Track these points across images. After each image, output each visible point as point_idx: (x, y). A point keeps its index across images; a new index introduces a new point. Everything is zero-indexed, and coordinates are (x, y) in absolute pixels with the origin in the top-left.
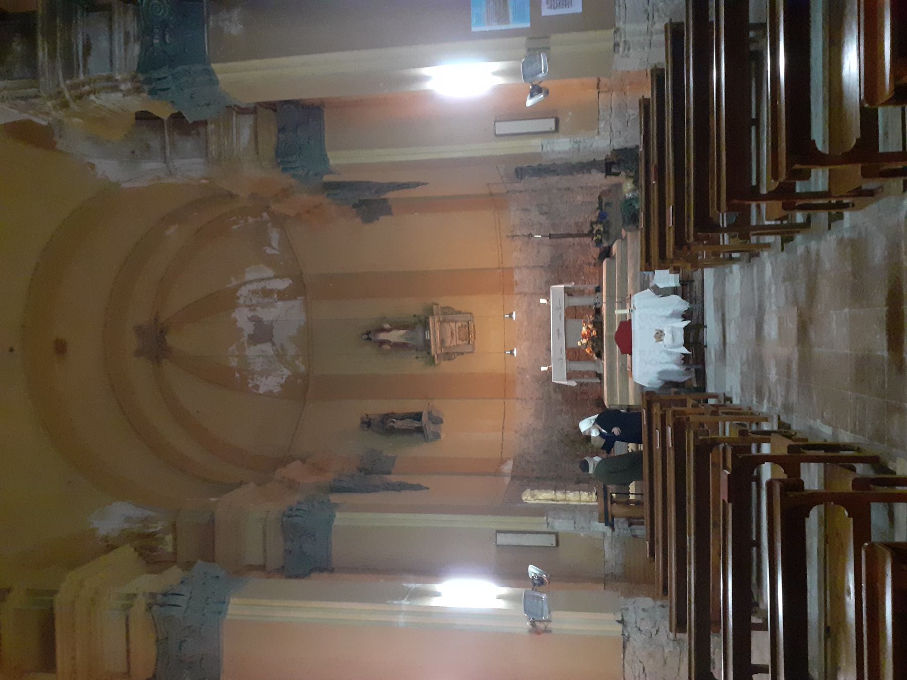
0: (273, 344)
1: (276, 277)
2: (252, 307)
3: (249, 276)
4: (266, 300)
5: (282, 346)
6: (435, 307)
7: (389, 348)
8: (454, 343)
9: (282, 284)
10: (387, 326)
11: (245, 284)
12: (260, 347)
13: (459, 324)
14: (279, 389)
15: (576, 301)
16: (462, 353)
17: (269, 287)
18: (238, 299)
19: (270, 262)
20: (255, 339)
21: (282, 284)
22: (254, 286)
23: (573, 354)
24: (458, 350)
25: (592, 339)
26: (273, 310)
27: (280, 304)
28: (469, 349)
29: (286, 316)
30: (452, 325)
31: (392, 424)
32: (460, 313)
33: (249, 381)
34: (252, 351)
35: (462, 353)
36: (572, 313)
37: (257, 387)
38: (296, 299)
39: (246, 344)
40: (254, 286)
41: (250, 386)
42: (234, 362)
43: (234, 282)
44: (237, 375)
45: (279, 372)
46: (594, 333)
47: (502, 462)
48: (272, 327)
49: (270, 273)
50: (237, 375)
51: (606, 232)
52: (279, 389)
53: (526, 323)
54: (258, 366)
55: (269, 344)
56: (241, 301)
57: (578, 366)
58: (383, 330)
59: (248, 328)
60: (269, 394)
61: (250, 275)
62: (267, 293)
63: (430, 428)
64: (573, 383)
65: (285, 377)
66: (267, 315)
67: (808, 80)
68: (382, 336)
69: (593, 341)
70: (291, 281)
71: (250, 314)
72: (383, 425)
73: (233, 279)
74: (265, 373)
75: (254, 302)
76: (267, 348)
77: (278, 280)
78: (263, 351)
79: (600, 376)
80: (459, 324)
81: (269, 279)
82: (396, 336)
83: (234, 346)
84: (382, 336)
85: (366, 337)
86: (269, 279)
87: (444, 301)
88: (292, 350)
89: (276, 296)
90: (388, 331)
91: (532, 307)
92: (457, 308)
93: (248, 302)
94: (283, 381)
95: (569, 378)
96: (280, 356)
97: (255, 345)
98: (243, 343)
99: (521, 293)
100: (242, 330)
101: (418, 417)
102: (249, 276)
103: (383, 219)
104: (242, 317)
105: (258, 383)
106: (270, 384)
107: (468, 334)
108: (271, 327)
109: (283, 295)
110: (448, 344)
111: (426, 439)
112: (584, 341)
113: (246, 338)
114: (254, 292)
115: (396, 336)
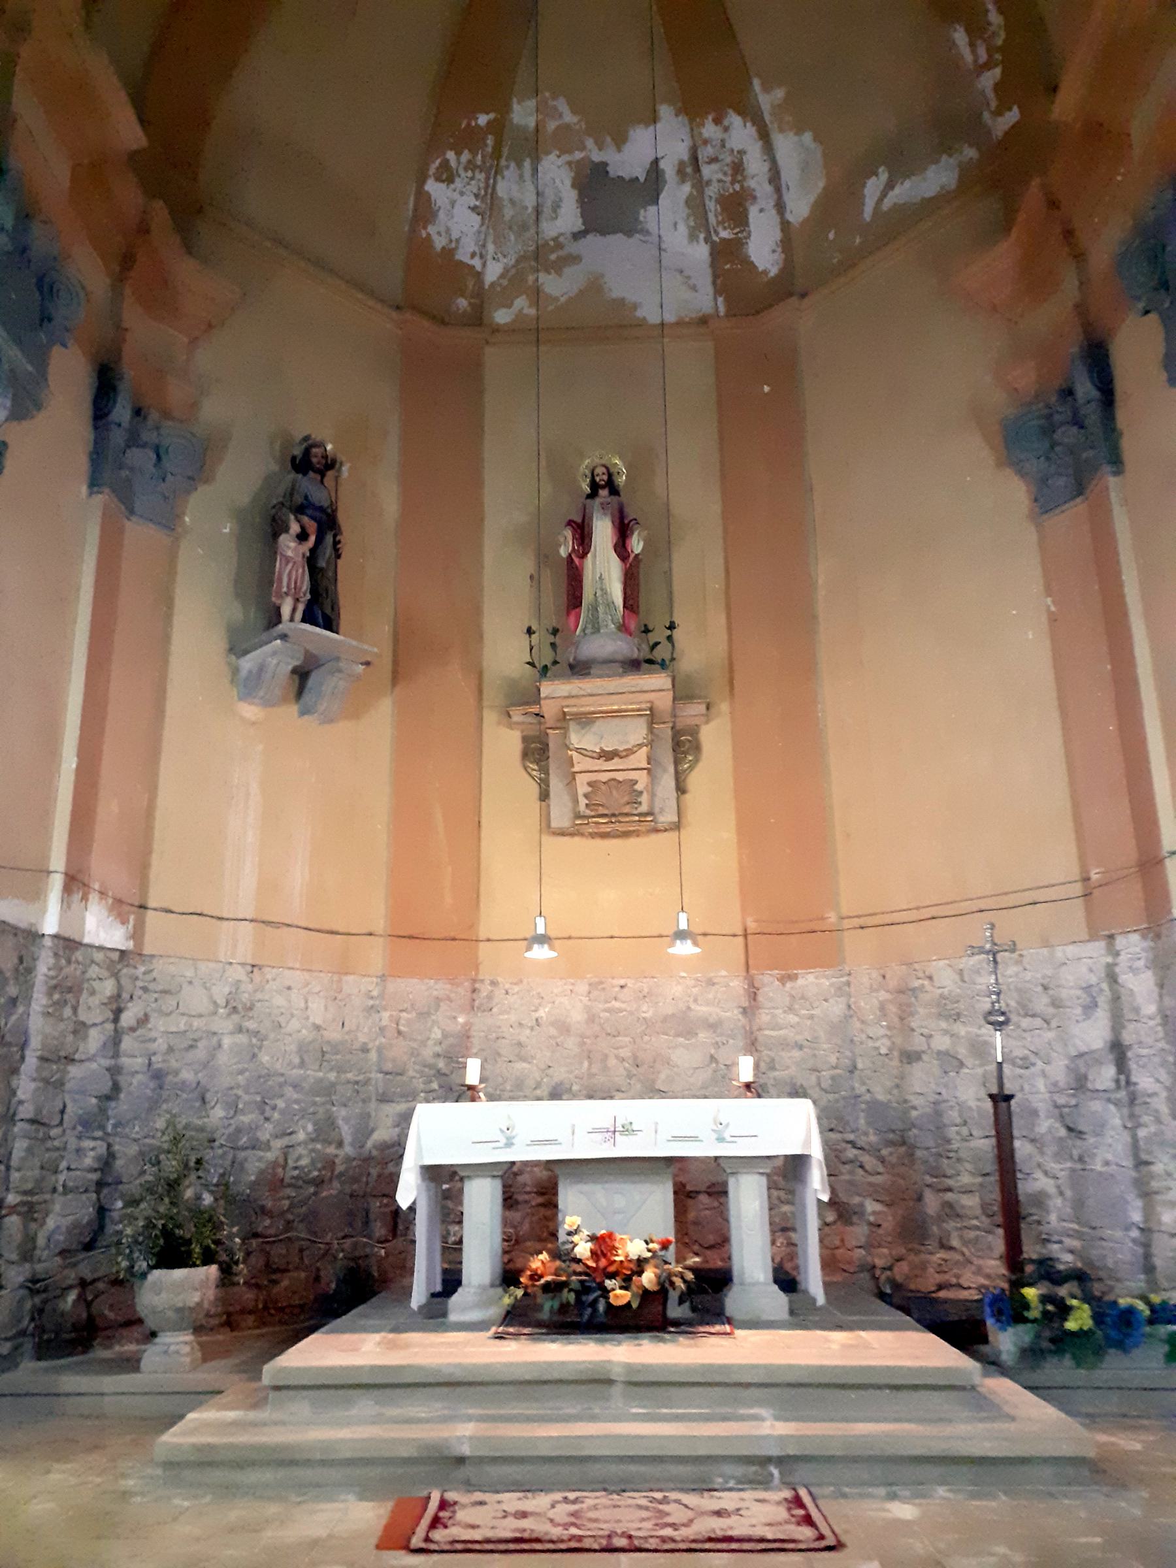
0: (577, 236)
1: (785, 225)
2: (692, 167)
3: (786, 145)
4: (711, 205)
5: (575, 259)
6: (698, 708)
7: (563, 552)
8: (580, 763)
9: (763, 250)
10: (636, 545)
11: (764, 135)
12: (570, 197)
13: (642, 779)
14: (439, 243)
15: (748, 1204)
16: (544, 796)
17: (753, 212)
18: (717, 121)
19: (836, 203)
20: (593, 183)
21: (763, 250)
22: (756, 165)
23: (532, 1194)
24: (556, 785)
25: (591, 1284)
26: (682, 229)
27: (701, 252)
28: (560, 816)
29: (665, 269)
30: (640, 758)
31: (295, 528)
32: (681, 789)
33: (466, 156)
34: (556, 173)
35: (544, 796)
36: (697, 1190)
37: (447, 176)
38: (718, 292)
39: (578, 155)
40: (756, 165)
41: (451, 155)
42: (523, 114)
43: (767, 100)
44: (483, 120)
45: (491, 247)
46: (620, 1296)
47: (132, 908)
48: (629, 233)
49: (799, 208)
50: (483, 120)
51: (1063, 1342)
52: (439, 243)
53: (647, 1010)
54: (513, 187)
55: (579, 225)
56: (709, 130)
57: (482, 1205)
58: (623, 531)
59: (629, 160)
60: (425, 211)
61: (790, 148)
62: (736, 207)
63: (275, 657)
64: (409, 1191)
65: (477, 263)
66: (668, 217)
67: (82, 738)
68: (603, 531)
69: (584, 1289)
70: (774, 271)
71: (668, 168)
72: (304, 503)
73: (779, 94)
74: (488, 205)
75: (707, 171)
76: (569, 218)
77: (778, 235)
78: (556, 207)
79: (435, 1313)
80: (642, 779)
81: (780, 207)
82: (604, 570)
83: (569, 118)
84: (603, 531)
85: (601, 478)
86: (780, 207)
87: (715, 738)
88: (558, 286)
89: (725, 234)
90: (621, 547)
91: (703, 1036)
92: (696, 780)
93: (705, 153)
94: (463, 256)
95: (434, 1174)
96: (544, 256)
97: (573, 186)
98: (583, 148)
99: (753, 993)
100: (620, 140)
101: (321, 610)
102: (786, 145)
103: (1016, 492)
104: (657, 141)
105: (458, 183)
106: (455, 216)
107: (613, 815)
108: (630, 227)
109: (728, 257)
110: (576, 738)
111: (237, 647)
112: (583, 1249)
113: (597, 157)
114: (738, 168)
115: (604, 570)
